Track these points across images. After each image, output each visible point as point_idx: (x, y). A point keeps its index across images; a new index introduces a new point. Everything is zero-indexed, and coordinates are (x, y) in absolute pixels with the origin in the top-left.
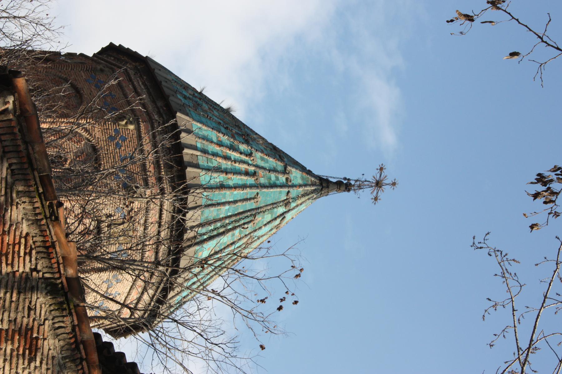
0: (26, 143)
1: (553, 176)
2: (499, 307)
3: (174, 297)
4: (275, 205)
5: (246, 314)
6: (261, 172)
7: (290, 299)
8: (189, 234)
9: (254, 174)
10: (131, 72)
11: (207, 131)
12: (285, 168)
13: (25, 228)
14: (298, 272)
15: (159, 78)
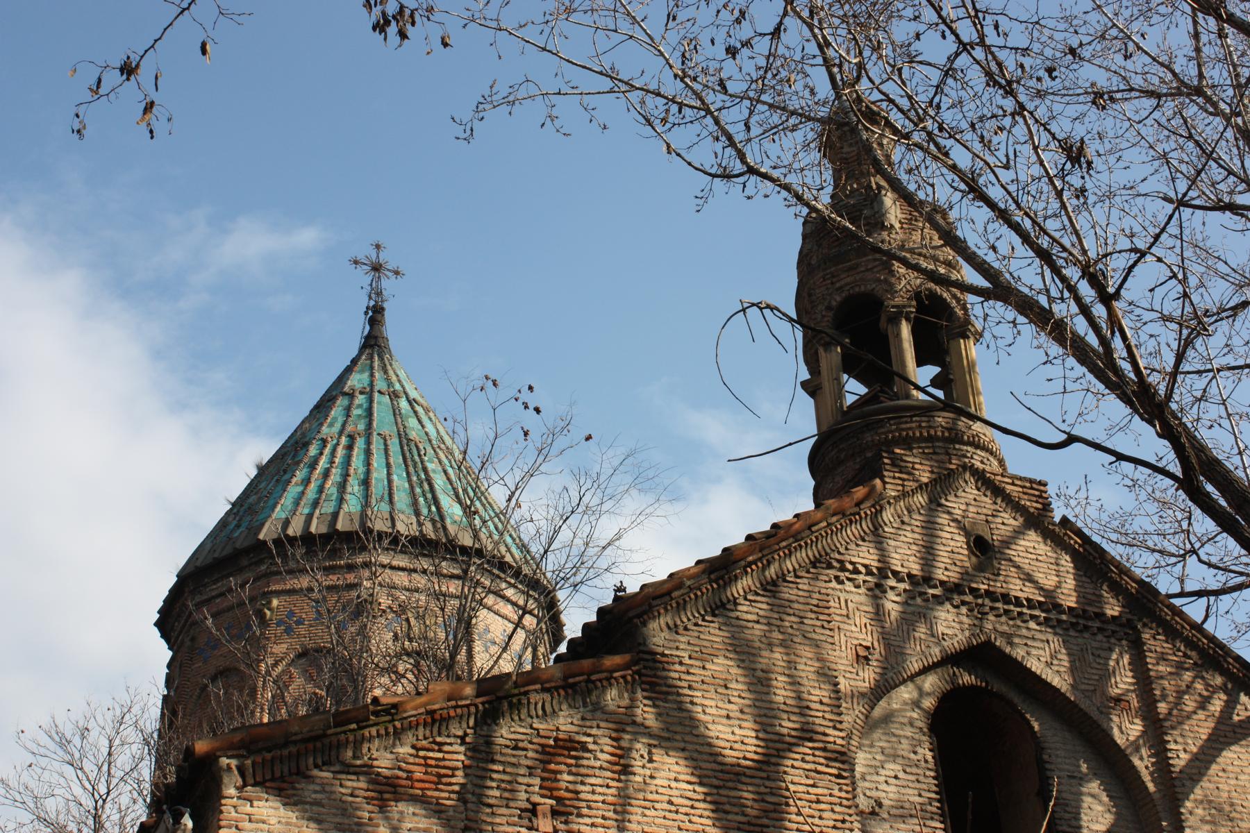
1: (377, 11)
2: (555, 112)
4: (396, 412)
5: (541, 458)
6: (349, 428)
7: (526, 396)
8: (428, 529)
9: (352, 438)
10: (198, 598)
13: (404, 750)
14: (490, 383)
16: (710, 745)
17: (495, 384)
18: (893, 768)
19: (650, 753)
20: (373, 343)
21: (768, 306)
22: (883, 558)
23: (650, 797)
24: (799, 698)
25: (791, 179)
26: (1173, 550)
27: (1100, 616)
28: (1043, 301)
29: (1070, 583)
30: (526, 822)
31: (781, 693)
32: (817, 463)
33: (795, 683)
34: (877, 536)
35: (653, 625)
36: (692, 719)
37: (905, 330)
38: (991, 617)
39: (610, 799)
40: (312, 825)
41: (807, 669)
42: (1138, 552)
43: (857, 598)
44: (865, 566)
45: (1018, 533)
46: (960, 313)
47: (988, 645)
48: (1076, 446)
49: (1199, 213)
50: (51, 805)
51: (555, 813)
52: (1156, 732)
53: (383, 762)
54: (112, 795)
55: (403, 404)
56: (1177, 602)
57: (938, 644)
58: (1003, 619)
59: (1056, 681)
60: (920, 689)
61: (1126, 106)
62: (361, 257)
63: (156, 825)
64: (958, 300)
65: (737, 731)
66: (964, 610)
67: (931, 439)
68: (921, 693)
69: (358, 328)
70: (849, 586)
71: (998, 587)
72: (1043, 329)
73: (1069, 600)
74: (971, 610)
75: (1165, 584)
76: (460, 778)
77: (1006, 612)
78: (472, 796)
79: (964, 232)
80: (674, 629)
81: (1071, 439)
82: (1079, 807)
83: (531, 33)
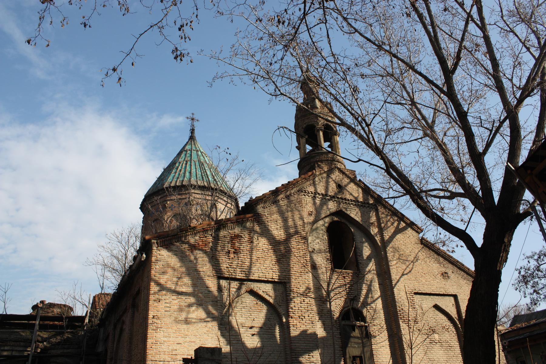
0: (168, 237)
1: (175, 54)
2: (233, 80)
3: (223, 188)
4: (198, 155)
5: (231, 166)
6: (186, 159)
7: (227, 150)
8: (206, 184)
9: (187, 161)
10: (150, 202)
11: (171, 177)
12: (185, 151)
13: (197, 238)
14: (218, 147)
15: (152, 192)
16: (273, 236)
17: (219, 147)
18: (318, 241)
19: (258, 238)
20: (192, 138)
21: (285, 128)
22: (316, 190)
23: (258, 248)
24: (295, 224)
25: (292, 96)
26: (386, 187)
27: (368, 203)
28: (353, 126)
29: (361, 195)
30: (227, 255)
31: (290, 223)
32: (300, 166)
33: (294, 220)
34: (314, 184)
35: (258, 207)
36: (268, 230)
37: (321, 134)
38: (342, 204)
39: (248, 249)
40: (175, 256)
41: (297, 217)
42: (378, 188)
43: (309, 200)
44: (311, 192)
45: (349, 183)
46: (335, 129)
47: (341, 211)
48: (361, 162)
49: (392, 105)
50: (115, 252)
51: (234, 253)
52: (381, 231)
53: (192, 241)
54: (129, 249)
55: (199, 153)
56: (387, 200)
57: (329, 210)
58: (345, 204)
59: (357, 219)
60: (325, 222)
61: (375, 79)
62: (189, 117)
63: (137, 256)
64: (334, 126)
65: (279, 232)
66: (335, 202)
67: (327, 160)
68: (325, 222)
69: (188, 134)
70: (307, 197)
71: (344, 197)
72: (353, 133)
73: (361, 199)
74: (337, 202)
75: (384, 196)
76: (211, 244)
77: (345, 203)
78: (214, 249)
79: (335, 110)
80: (264, 208)
81: (360, 160)
82: (363, 249)
83: (227, 60)
